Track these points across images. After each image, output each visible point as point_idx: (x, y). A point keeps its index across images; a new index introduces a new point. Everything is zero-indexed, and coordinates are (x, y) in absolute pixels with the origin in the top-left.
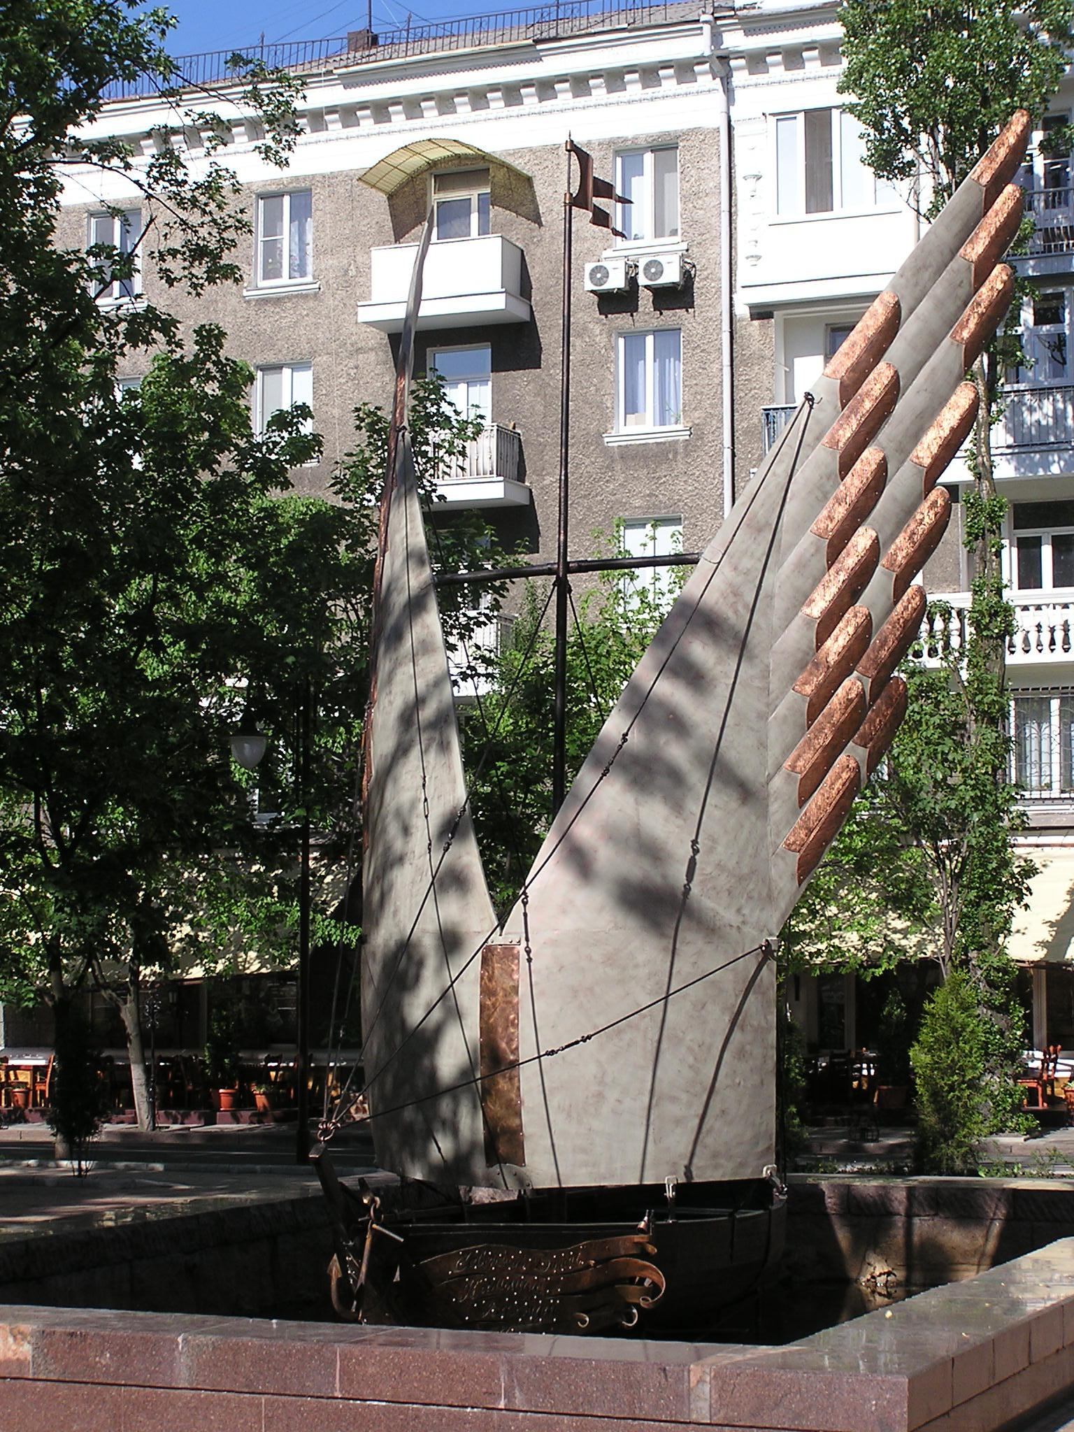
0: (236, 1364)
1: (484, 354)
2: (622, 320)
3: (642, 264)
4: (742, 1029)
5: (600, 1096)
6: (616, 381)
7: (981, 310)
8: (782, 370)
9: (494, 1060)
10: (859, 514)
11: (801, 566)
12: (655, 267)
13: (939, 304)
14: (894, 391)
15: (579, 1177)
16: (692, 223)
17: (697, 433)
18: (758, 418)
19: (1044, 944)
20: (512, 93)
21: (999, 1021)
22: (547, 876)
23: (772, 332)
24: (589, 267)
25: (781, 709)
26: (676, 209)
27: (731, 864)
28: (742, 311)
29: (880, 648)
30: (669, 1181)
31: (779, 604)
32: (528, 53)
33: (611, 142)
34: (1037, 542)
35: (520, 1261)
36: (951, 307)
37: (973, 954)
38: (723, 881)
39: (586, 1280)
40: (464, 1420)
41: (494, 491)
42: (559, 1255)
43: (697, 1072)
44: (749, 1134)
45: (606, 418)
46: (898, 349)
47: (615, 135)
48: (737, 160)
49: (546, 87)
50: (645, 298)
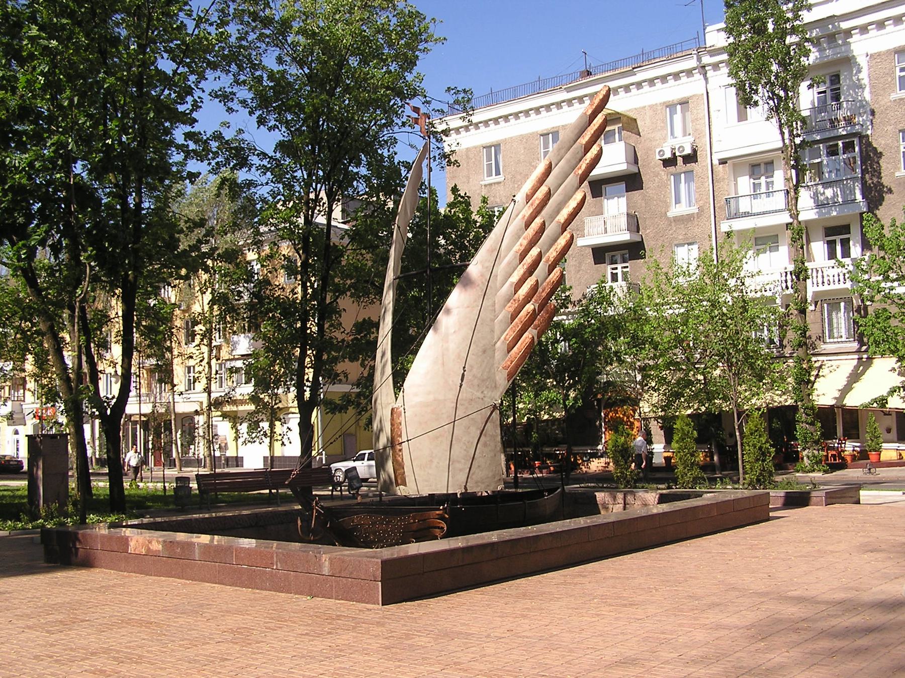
1: (623, 186)
2: (672, 169)
5: (431, 461)
6: (671, 192)
7: (588, 161)
10: (532, 243)
11: (509, 263)
12: (681, 148)
13: (569, 161)
14: (548, 196)
19: (835, 398)
23: (727, 169)
25: (500, 317)
26: (690, 126)
27: (479, 375)
28: (715, 162)
29: (542, 293)
30: (459, 492)
32: (631, 73)
33: (664, 103)
34: (835, 241)
35: (384, 519)
36: (574, 162)
38: (476, 382)
39: (415, 527)
44: (491, 474)
45: (667, 207)
49: (639, 85)
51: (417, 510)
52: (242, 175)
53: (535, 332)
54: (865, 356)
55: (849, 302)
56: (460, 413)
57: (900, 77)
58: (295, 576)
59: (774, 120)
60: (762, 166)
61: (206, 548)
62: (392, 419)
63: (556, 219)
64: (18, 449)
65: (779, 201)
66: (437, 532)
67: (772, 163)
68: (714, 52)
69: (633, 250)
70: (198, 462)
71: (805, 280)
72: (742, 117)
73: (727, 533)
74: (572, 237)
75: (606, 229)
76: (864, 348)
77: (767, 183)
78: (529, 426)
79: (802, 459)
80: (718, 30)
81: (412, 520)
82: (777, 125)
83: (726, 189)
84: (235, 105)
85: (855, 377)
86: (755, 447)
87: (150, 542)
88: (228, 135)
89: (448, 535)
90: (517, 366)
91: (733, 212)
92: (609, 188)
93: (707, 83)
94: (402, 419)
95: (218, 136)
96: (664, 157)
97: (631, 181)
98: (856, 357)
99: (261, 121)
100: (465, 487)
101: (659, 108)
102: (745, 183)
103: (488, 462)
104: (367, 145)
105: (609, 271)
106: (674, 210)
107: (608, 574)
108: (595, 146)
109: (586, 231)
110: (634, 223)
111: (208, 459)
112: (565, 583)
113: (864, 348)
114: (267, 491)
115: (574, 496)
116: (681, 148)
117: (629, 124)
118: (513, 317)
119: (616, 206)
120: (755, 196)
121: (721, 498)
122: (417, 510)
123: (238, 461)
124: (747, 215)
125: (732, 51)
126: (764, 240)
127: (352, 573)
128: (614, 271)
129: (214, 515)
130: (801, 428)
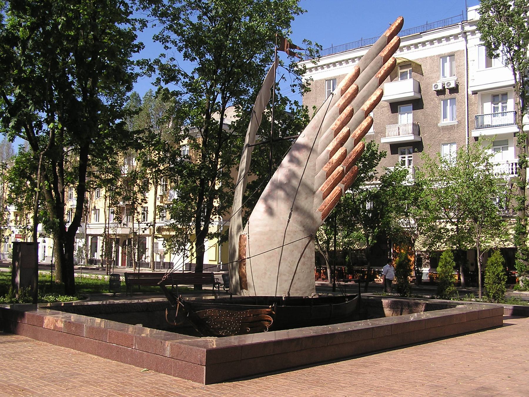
0: (93, 332)
2: (442, 97)
4: (304, 257)
7: (385, 69)
8: (480, 106)
10: (344, 124)
11: (327, 137)
13: (372, 68)
14: (357, 91)
15: (260, 294)
16: (458, 73)
18: (474, 118)
20: (416, 46)
23: (477, 97)
24: (433, 85)
28: (470, 93)
29: (350, 158)
30: (283, 296)
33: (439, 55)
36: (376, 69)
37: (518, 246)
40: (127, 350)
41: (411, 138)
42: (240, 313)
43: (291, 268)
44: (306, 285)
45: (438, 120)
46: (358, 81)
47: (440, 54)
48: (469, 57)
49: (424, 44)
50: (447, 91)
51: (252, 308)
52: (172, 87)
53: (343, 186)
56: (287, 241)
58: (147, 356)
59: (510, 66)
60: (500, 97)
61: (92, 329)
62: (240, 243)
63: (362, 108)
64: (45, 252)
65: (510, 118)
66: (267, 325)
67: (506, 94)
68: (471, 24)
69: (416, 146)
70: (147, 265)
71: (525, 168)
72: (489, 65)
73: (473, 335)
74: (372, 121)
75: (399, 132)
77: (503, 107)
78: (345, 252)
79: (519, 282)
80: (476, 10)
81: (249, 314)
82: (511, 69)
83: (476, 110)
84: (169, 45)
86: (494, 274)
87: (57, 321)
88: (164, 61)
89: (272, 329)
90: (329, 209)
91: (480, 124)
92: (402, 108)
94: (247, 243)
95: (157, 62)
96: (438, 89)
97: (416, 103)
99: (186, 56)
100: (289, 292)
101: (436, 58)
102: (488, 107)
103: (305, 276)
104: (254, 74)
105: (400, 159)
106: (443, 122)
107: (385, 365)
108: (391, 59)
109: (387, 134)
110: (417, 129)
111: (152, 263)
112: (351, 372)
115: (368, 301)
117: (415, 68)
118: (328, 175)
119: (406, 119)
120: (494, 115)
121: (471, 309)
122: (252, 308)
123: (170, 265)
124: (489, 126)
126: (499, 143)
127: (185, 357)
128: (403, 159)
129: (104, 303)
130: (519, 262)
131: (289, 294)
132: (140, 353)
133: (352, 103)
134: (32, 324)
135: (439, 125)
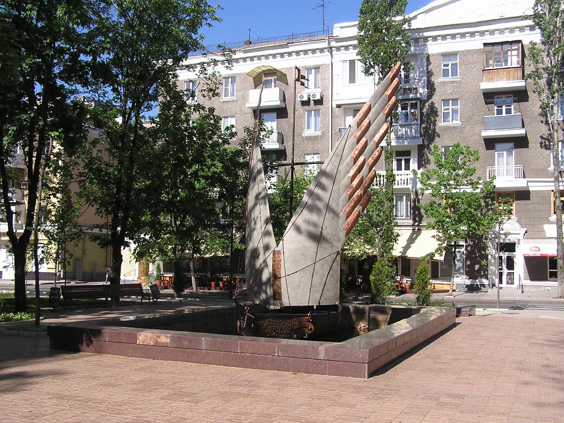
2: (307, 107)
3: (311, 95)
5: (299, 285)
9: (275, 277)
10: (361, 153)
11: (347, 164)
12: (314, 95)
13: (380, 105)
14: (369, 125)
15: (294, 304)
17: (323, 133)
18: (337, 130)
19: (401, 252)
21: (390, 270)
22: (289, 234)
23: (341, 111)
24: (299, 95)
28: (334, 106)
29: (365, 183)
30: (315, 305)
31: (342, 173)
32: (286, 46)
33: (305, 67)
34: (401, 160)
35: (281, 322)
36: (383, 106)
39: (296, 327)
41: (276, 146)
45: (302, 130)
47: (305, 65)
49: (290, 54)
53: (361, 208)
54: (417, 228)
55: (408, 196)
57: (443, 69)
76: (416, 224)
85: (411, 240)
93: (332, 58)
98: (412, 228)
104: (163, 76)
113: (416, 224)
114: (104, 299)
116: (314, 95)
125: (361, 40)
131: (319, 303)
132: (284, 359)
133: (366, 135)
134: (117, 341)
135: (303, 134)
